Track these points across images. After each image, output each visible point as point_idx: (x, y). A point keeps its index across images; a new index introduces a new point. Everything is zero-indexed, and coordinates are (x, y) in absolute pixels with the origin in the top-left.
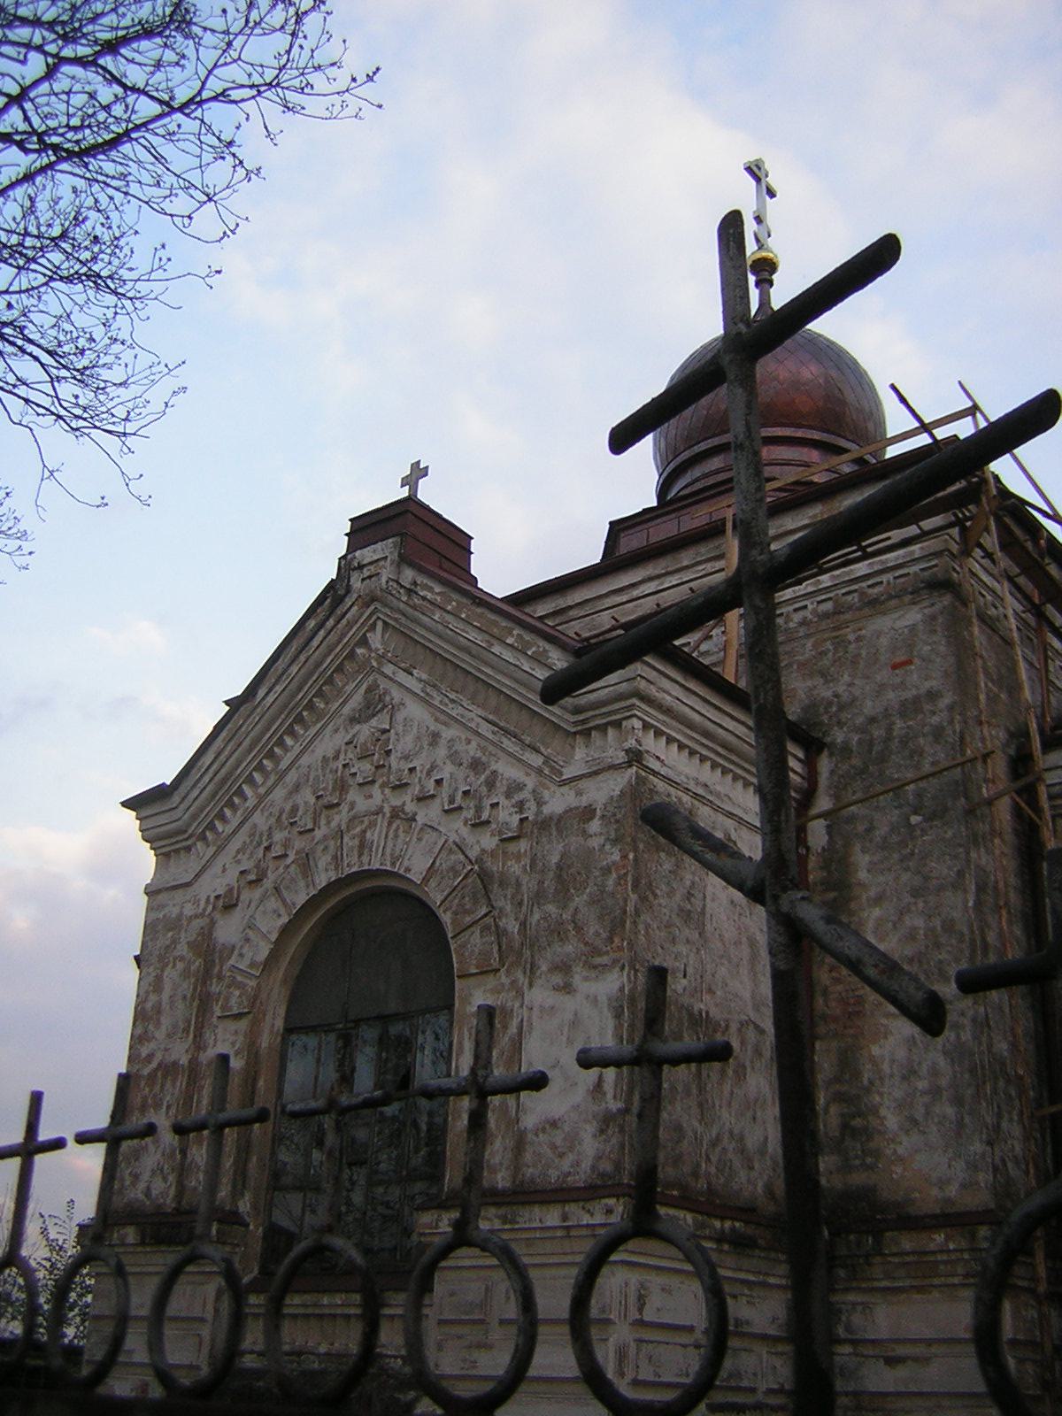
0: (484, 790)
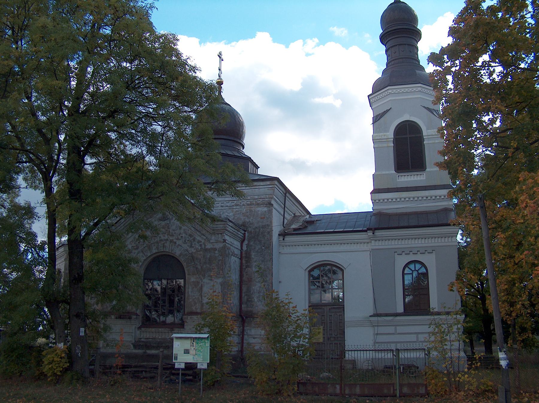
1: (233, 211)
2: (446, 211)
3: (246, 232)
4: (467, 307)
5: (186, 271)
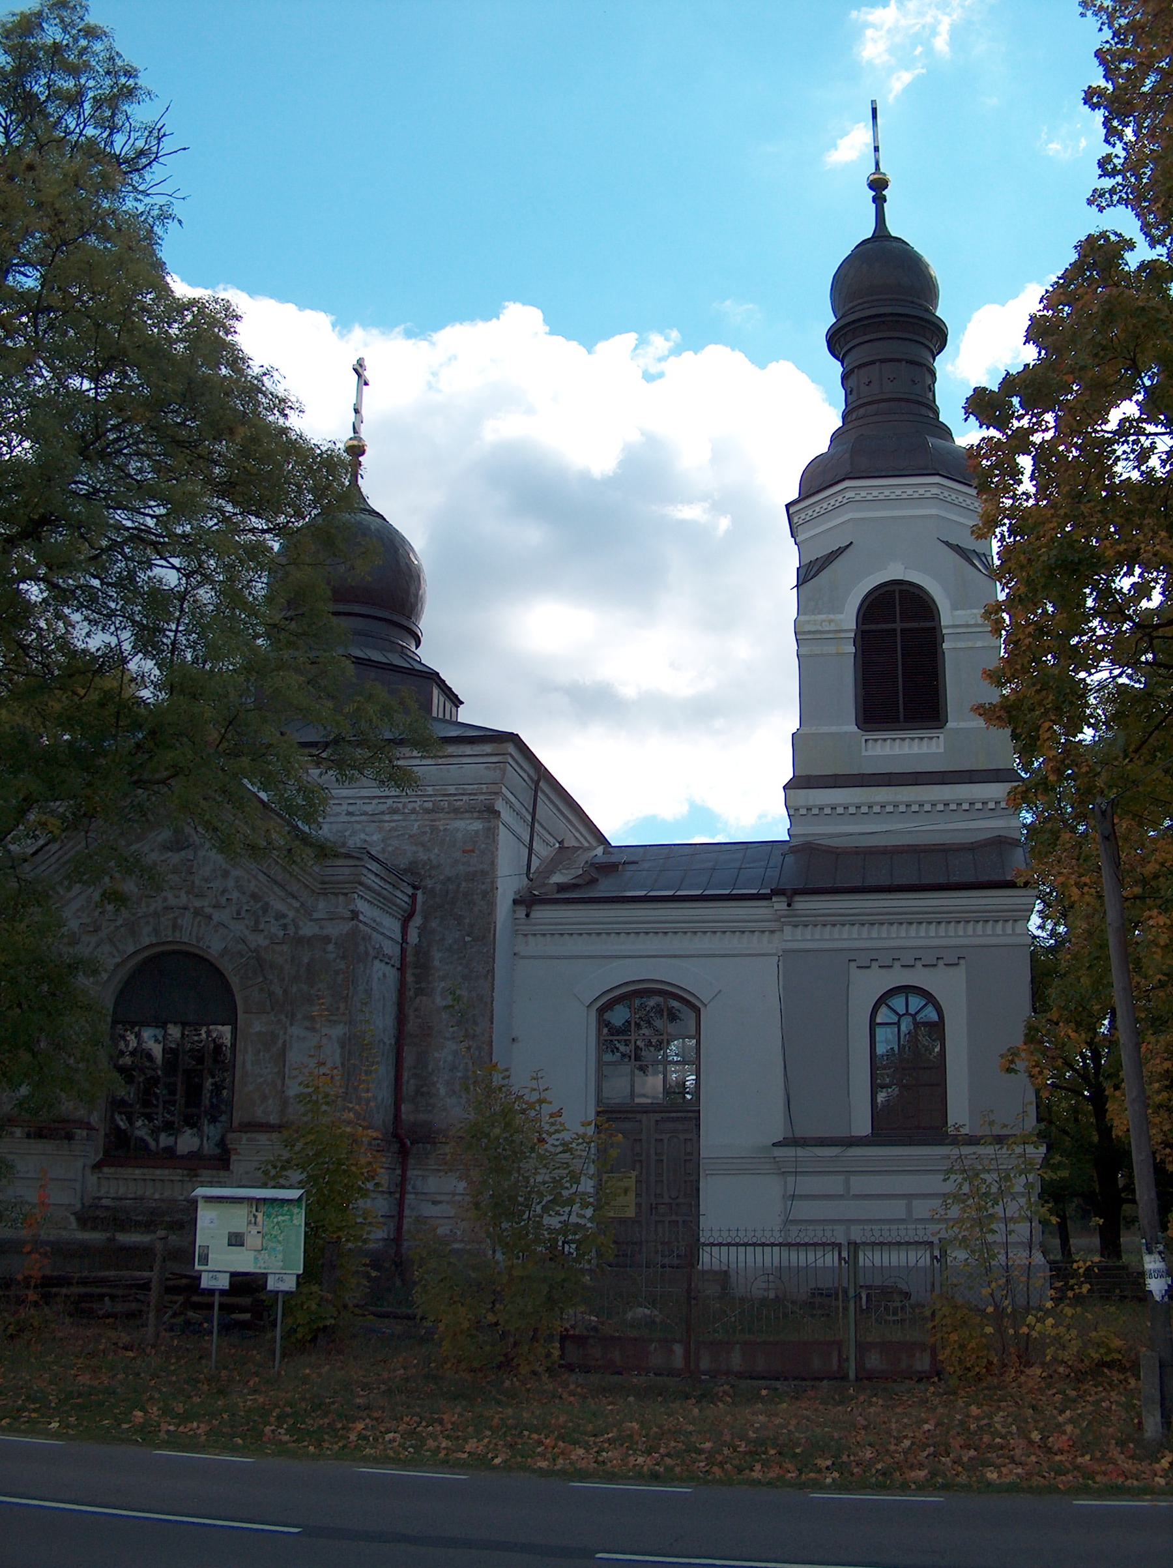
0: (260, 912)
2: (1002, 844)
3: (419, 892)
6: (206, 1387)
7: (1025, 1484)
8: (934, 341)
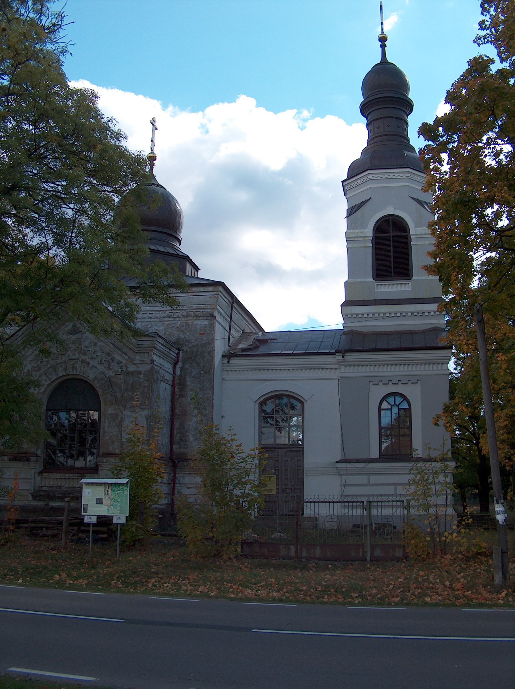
0: (111, 361)
1: (164, 324)
2: (436, 330)
3: (181, 352)
4: (459, 454)
5: (102, 401)
6: (87, 565)
7: (442, 603)
8: (407, 109)
